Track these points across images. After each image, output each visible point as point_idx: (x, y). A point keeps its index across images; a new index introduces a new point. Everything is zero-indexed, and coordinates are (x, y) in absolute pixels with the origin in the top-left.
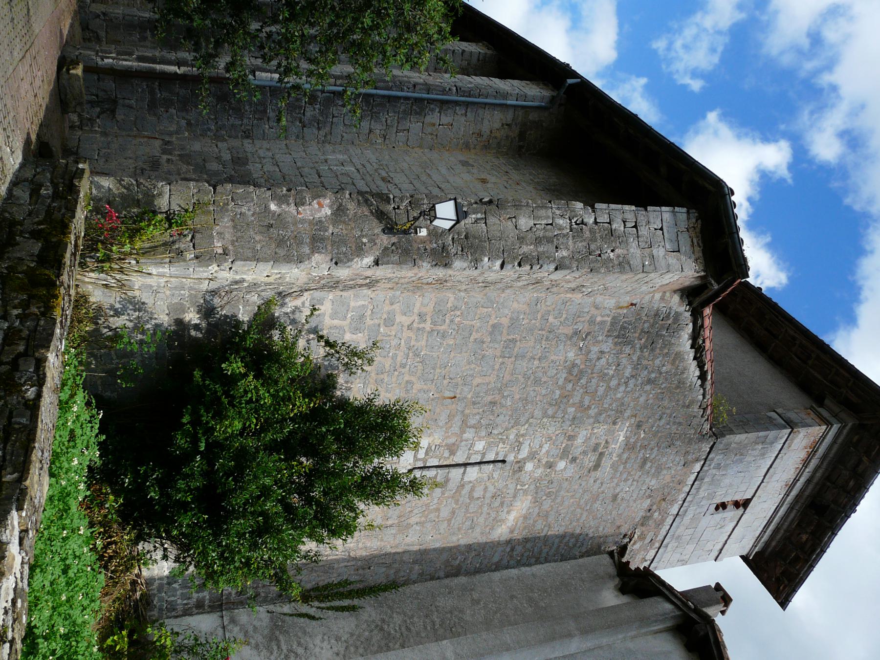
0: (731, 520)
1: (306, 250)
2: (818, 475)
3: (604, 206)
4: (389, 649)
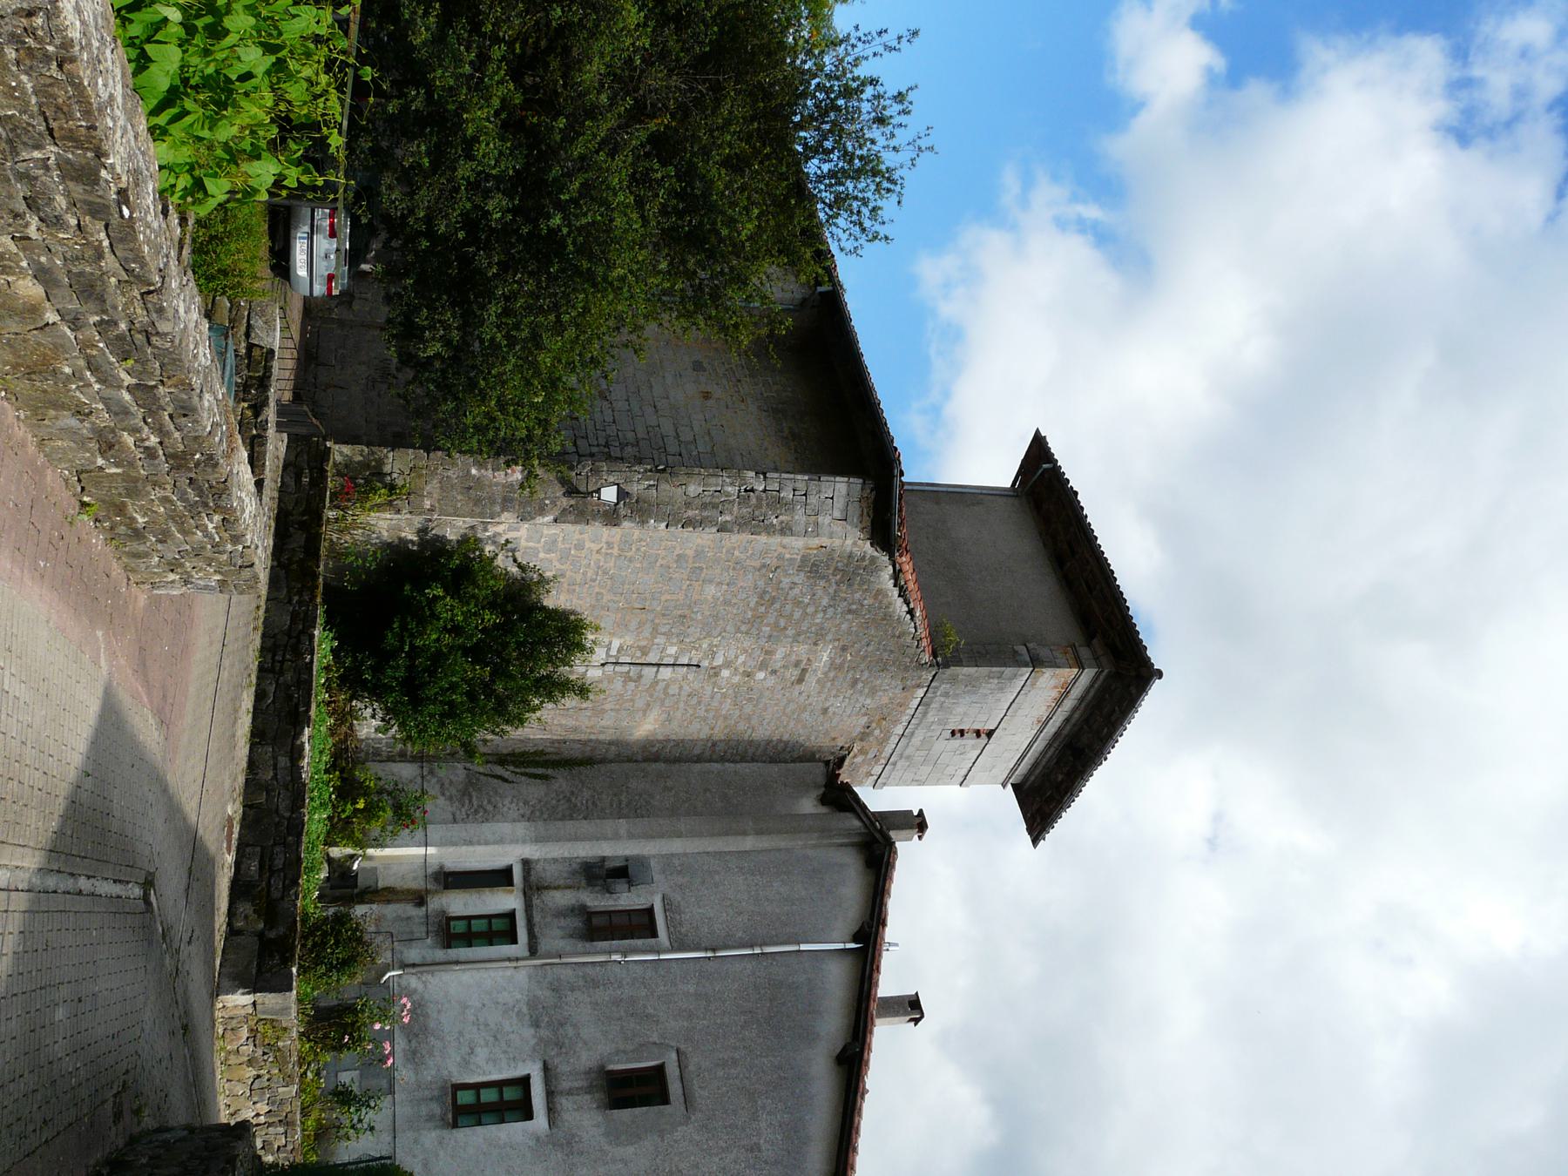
0: (974, 748)
1: (498, 509)
2: (1076, 716)
3: (776, 475)
4: (572, 818)
